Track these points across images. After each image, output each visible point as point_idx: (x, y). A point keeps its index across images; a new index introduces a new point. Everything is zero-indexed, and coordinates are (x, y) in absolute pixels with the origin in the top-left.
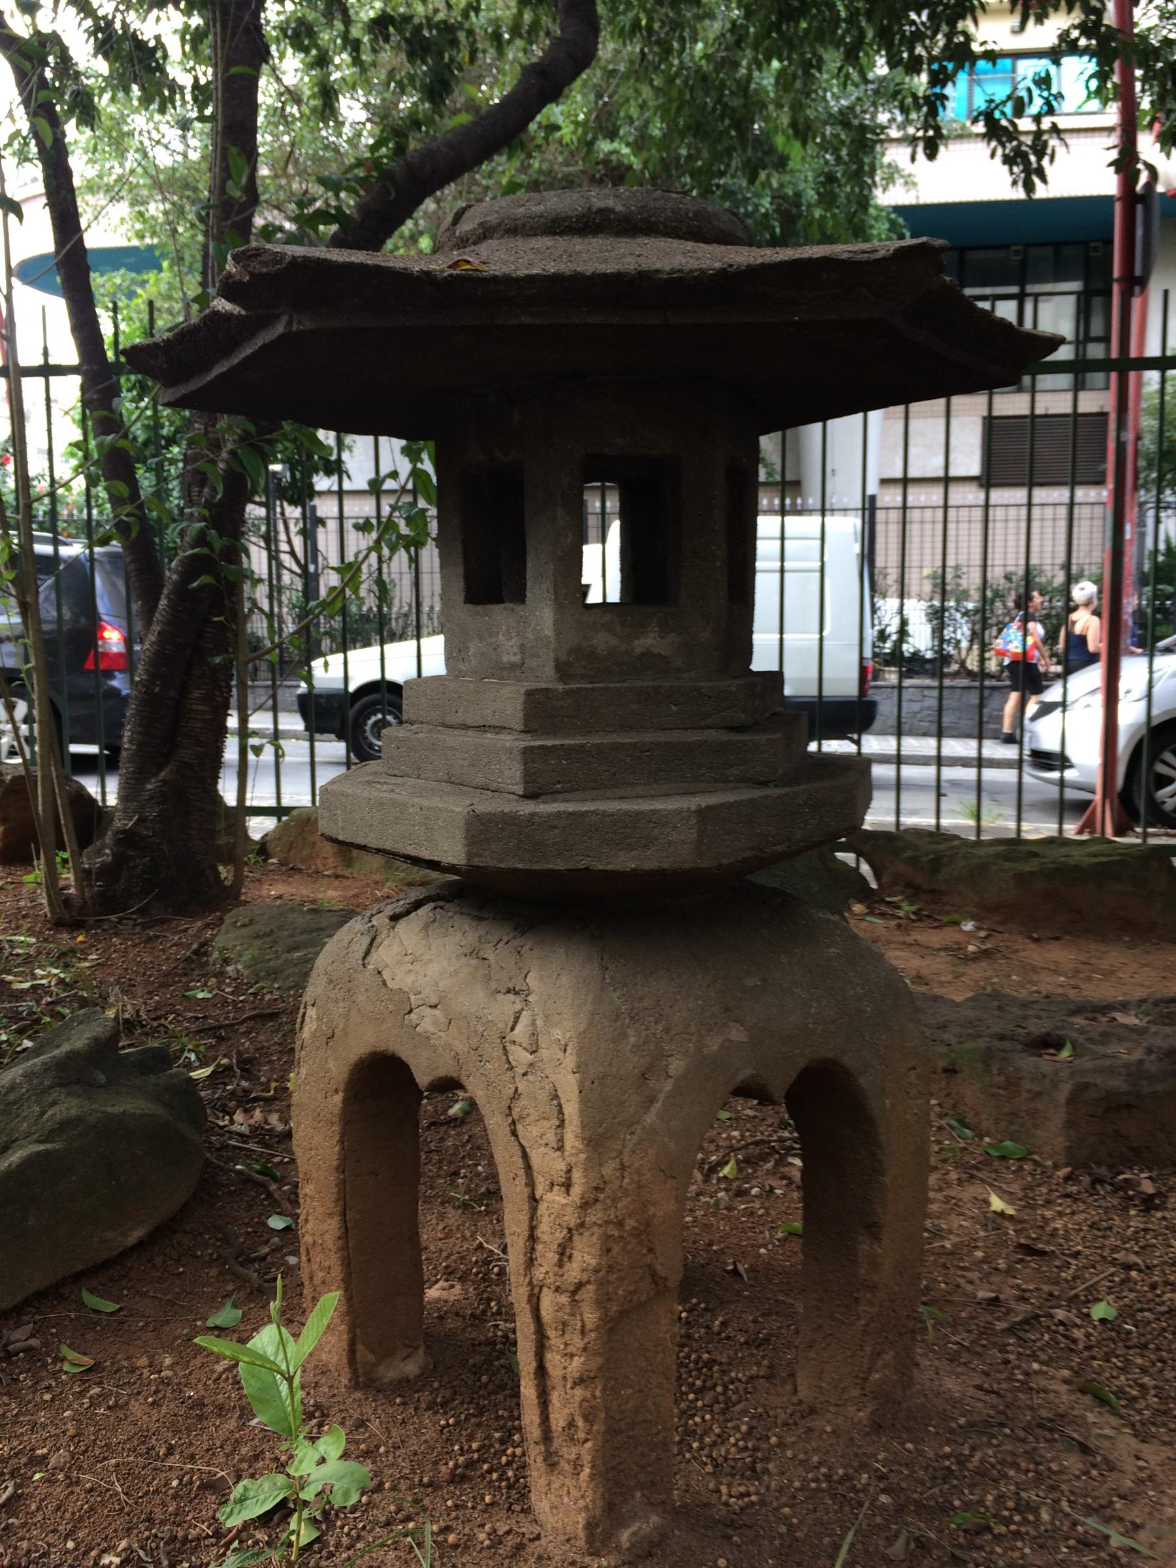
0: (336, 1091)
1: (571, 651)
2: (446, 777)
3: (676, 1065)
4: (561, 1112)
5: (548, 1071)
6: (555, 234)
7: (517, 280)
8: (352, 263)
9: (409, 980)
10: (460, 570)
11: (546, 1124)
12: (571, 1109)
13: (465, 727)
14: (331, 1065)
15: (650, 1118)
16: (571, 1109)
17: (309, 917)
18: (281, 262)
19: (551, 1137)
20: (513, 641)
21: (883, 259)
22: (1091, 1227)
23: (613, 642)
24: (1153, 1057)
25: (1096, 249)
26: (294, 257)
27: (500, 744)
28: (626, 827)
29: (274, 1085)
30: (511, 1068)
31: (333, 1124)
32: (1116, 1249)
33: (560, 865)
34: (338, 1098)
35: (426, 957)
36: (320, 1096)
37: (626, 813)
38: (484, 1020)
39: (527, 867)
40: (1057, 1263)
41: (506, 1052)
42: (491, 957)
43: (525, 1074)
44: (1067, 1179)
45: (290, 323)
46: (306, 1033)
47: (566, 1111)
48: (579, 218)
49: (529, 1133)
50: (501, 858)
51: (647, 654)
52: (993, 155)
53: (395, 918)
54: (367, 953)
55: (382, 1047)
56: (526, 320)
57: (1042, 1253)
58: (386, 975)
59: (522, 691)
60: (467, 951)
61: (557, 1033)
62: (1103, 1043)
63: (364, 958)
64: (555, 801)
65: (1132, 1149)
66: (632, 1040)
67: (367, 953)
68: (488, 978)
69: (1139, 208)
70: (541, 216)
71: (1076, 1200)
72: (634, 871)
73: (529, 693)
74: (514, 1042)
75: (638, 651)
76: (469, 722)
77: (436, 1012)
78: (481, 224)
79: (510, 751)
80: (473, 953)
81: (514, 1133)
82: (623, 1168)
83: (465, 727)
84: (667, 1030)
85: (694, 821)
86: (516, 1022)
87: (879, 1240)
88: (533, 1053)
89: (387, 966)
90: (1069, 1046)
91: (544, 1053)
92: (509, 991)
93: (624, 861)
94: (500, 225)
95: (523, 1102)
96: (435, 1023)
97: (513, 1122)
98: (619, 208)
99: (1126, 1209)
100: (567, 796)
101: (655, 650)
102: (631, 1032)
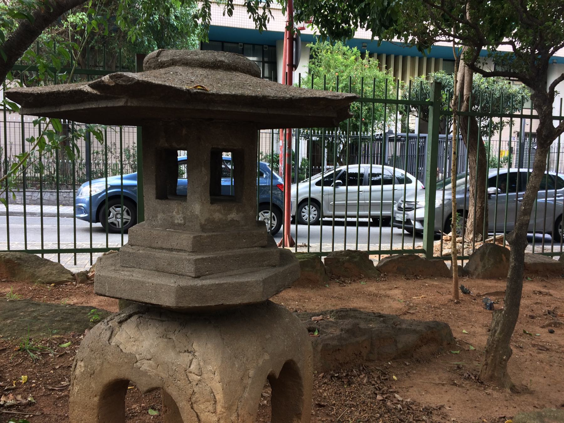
0: (96, 396)
1: (206, 220)
2: (155, 269)
3: (251, 373)
4: (215, 398)
5: (207, 383)
6: (202, 67)
7: (221, 95)
8: (165, 86)
9: (134, 349)
10: (154, 186)
11: (209, 403)
12: (219, 397)
13: (162, 249)
14: (93, 385)
15: (246, 395)
16: (219, 397)
17: (10, 304)
18: (131, 81)
19: (211, 408)
20: (180, 215)
21: (341, 99)
22: (335, 393)
23: (221, 216)
24: (343, 332)
25: (266, 48)
26: (138, 80)
27: (184, 257)
28: (238, 288)
29: (14, 382)
30: (190, 383)
31: (94, 409)
32: (345, 401)
33: (213, 304)
34: (96, 399)
35: (141, 339)
36: (87, 399)
37: (238, 283)
38: (176, 364)
39: (200, 305)
40: (330, 409)
41: (187, 377)
42: (174, 338)
43: (197, 384)
44: (323, 377)
45: (126, 102)
46: (77, 372)
47: (217, 398)
48: (212, 63)
49: (200, 407)
50: (187, 303)
51: (232, 220)
52: (250, 18)
53: (121, 323)
54: (110, 338)
55: (122, 377)
56: (220, 109)
57: (323, 406)
58: (121, 347)
59: (192, 237)
60: (161, 335)
61: (210, 368)
62: (327, 329)
63: (109, 341)
64: (206, 279)
65: (340, 364)
66: (237, 366)
67: (110, 338)
68: (174, 347)
69: (294, 42)
70: (198, 60)
71: (328, 384)
72: (240, 304)
73: (195, 237)
74: (191, 372)
75: (229, 219)
76: (164, 247)
77: (151, 362)
78: (171, 59)
79: (189, 260)
80: (164, 336)
81: (192, 408)
82: (238, 415)
83: (162, 249)
84: (247, 360)
85: (262, 284)
86: (190, 364)
87: (300, 419)
88: (200, 376)
89: (121, 343)
90: (317, 331)
91: (205, 376)
92: (185, 352)
93: (237, 301)
94: (180, 61)
95: (197, 396)
96: (150, 366)
97: (192, 404)
98: (226, 61)
99: (343, 385)
100: (211, 276)
101: (235, 219)
102: (236, 363)
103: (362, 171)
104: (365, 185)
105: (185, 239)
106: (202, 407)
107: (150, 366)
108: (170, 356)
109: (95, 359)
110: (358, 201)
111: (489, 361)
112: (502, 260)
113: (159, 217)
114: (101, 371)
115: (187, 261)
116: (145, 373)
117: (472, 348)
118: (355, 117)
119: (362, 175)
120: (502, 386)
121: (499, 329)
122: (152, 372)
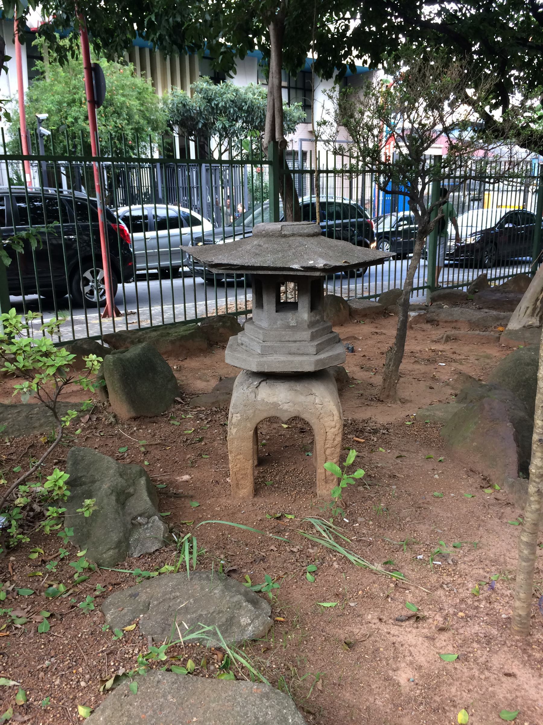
91: (325, 404)
103: (146, 213)
104: (151, 230)
105: (306, 335)
106: (326, 419)
107: (290, 406)
108: (301, 399)
109: (249, 410)
110: (146, 250)
111: (386, 386)
112: (340, 308)
113: (279, 322)
114: (254, 416)
115: (311, 347)
116: (286, 411)
117: (359, 382)
118: (118, 140)
119: (146, 217)
120: (395, 402)
121: (392, 363)
122: (292, 409)
